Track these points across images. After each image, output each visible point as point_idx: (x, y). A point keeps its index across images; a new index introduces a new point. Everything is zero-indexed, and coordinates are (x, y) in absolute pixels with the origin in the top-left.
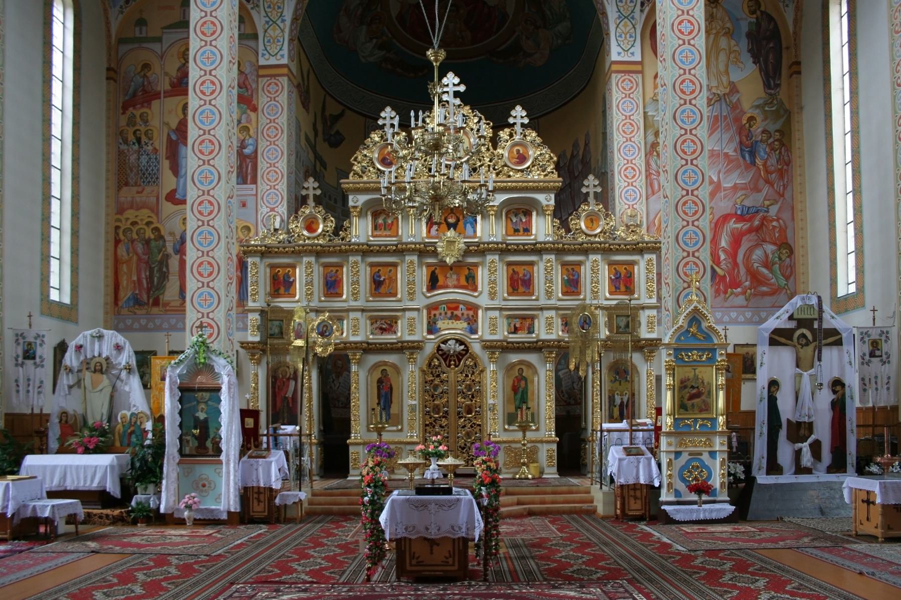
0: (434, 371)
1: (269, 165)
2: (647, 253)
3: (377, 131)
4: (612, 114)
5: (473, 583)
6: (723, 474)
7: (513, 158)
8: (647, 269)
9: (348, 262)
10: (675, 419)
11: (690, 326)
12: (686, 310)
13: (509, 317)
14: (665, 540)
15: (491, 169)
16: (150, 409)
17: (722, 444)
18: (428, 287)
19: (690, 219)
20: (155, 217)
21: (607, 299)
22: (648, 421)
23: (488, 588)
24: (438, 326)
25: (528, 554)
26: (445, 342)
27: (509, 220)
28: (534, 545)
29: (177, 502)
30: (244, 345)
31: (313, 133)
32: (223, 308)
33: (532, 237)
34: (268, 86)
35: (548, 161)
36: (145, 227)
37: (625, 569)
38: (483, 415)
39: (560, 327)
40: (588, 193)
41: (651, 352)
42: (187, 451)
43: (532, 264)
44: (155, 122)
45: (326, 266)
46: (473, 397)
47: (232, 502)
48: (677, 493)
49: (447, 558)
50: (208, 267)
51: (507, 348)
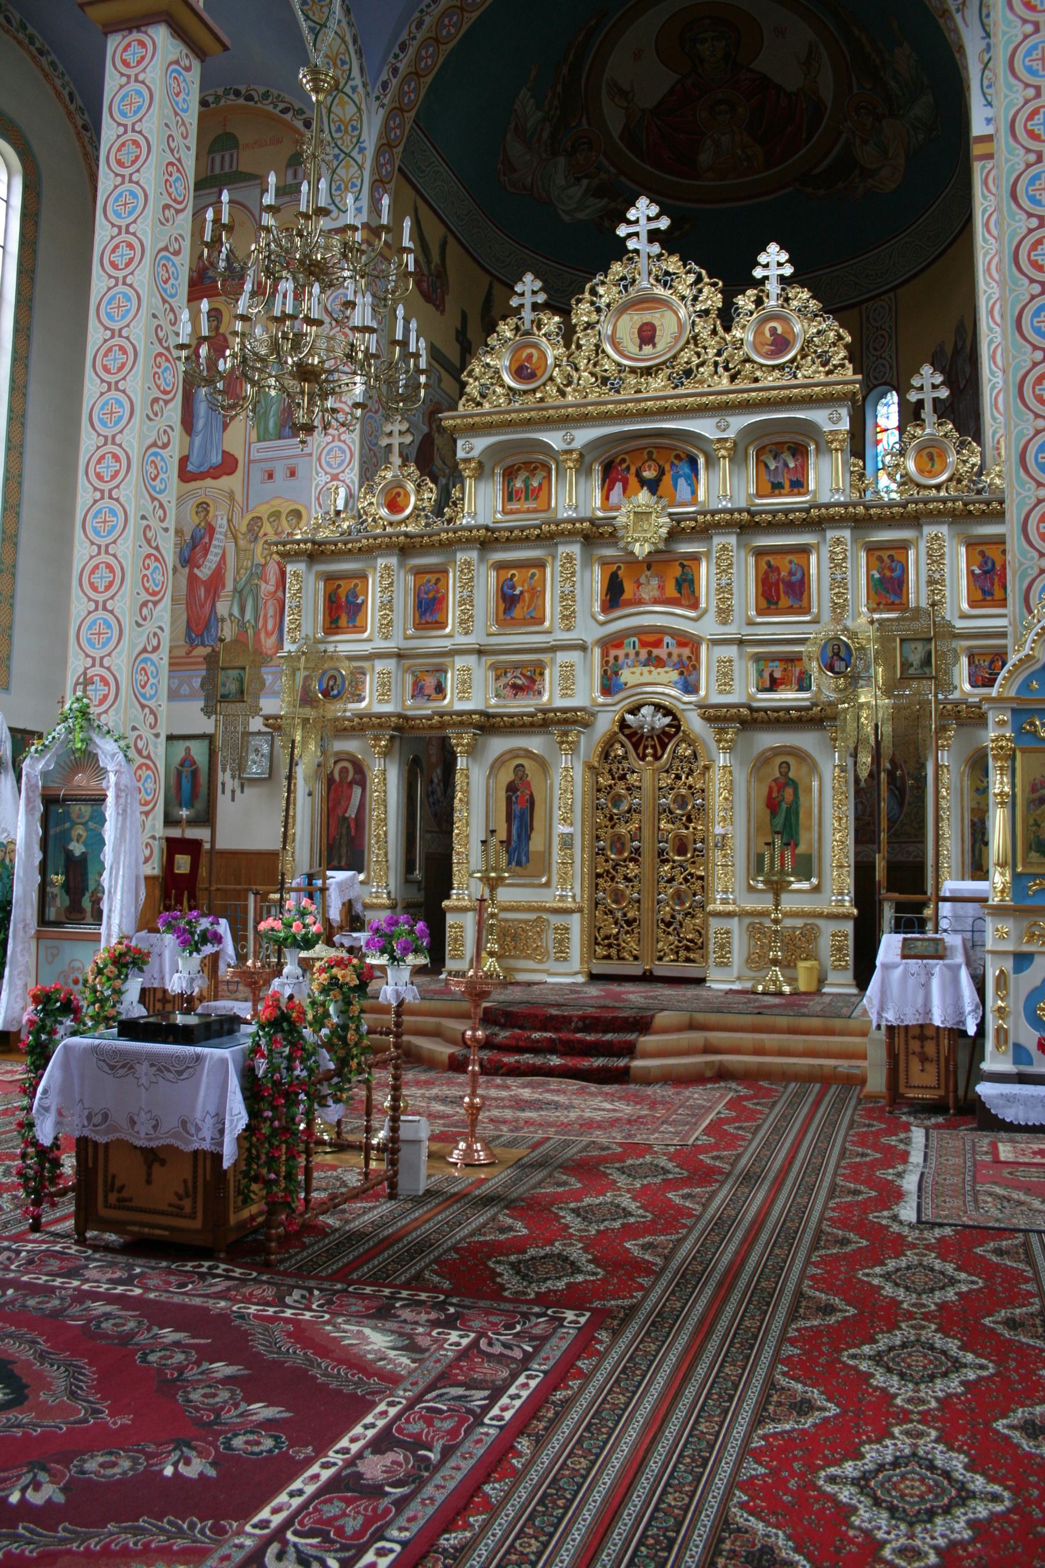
0: (614, 767)
3: (509, 320)
7: (763, 344)
10: (1016, 876)
13: (757, 658)
15: (720, 370)
18: (603, 602)
21: (964, 616)
27: (762, 467)
31: (458, 347)
35: (834, 344)
43: (804, 550)
45: (418, 572)
48: (1020, 1054)
49: (181, 1199)
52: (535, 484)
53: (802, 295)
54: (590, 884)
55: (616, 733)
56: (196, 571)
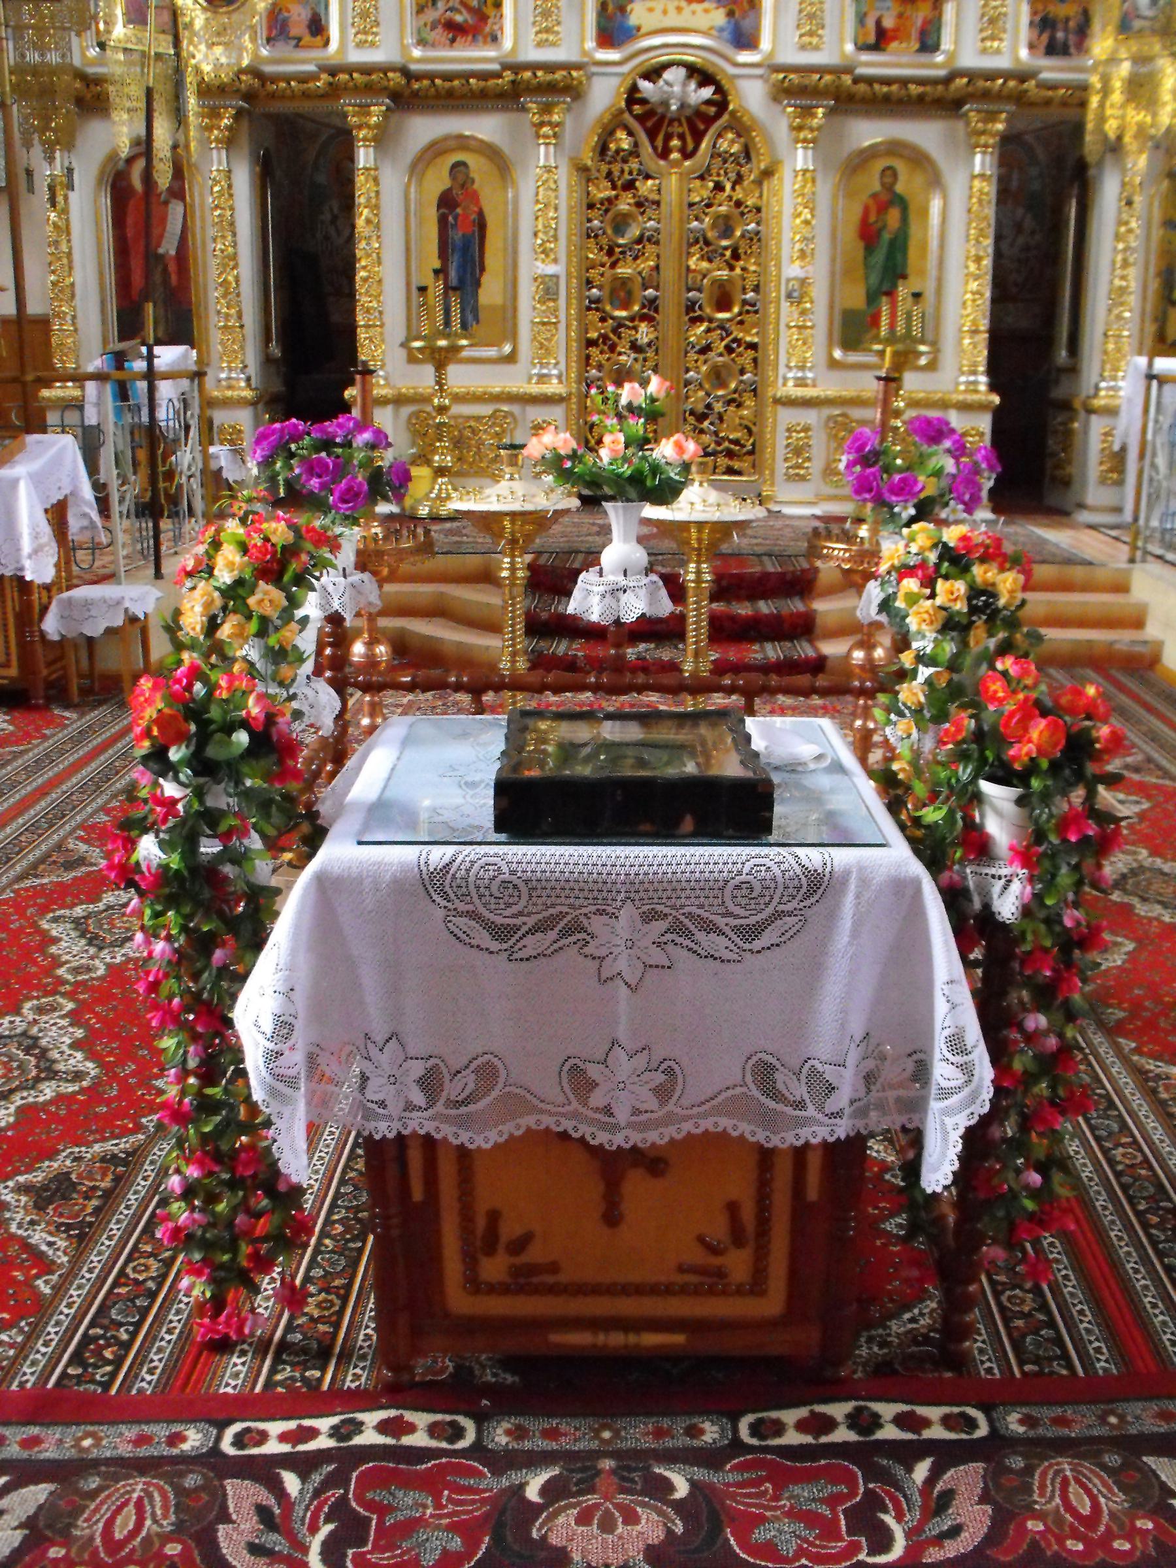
0: (616, 168)
26: (653, 73)
38: (766, 315)
46: (736, 256)
54: (579, 356)
55: (621, 112)
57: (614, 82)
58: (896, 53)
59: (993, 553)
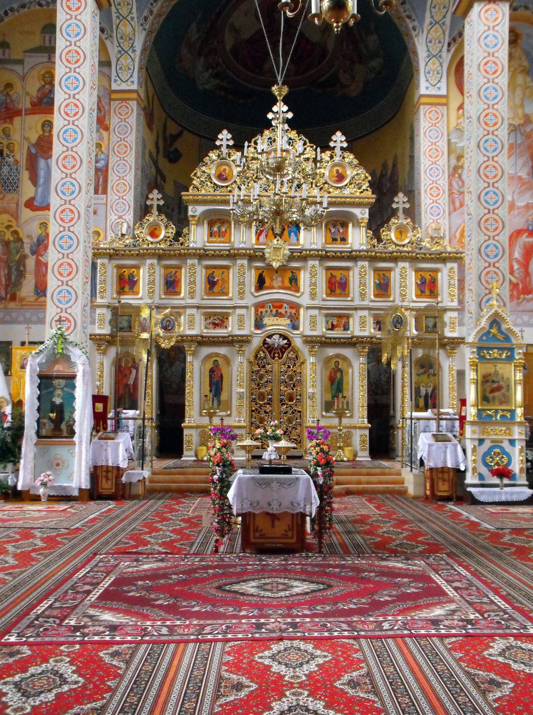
0: (260, 362)
1: (118, 178)
2: (449, 262)
4: (419, 140)
5: (310, 554)
6: (522, 461)
8: (450, 276)
9: (186, 264)
10: (478, 410)
11: (491, 327)
12: (487, 314)
13: (326, 316)
14: (473, 519)
16: (10, 394)
17: (520, 433)
19: (492, 234)
20: (14, 221)
22: (451, 411)
23: (324, 558)
24: (264, 322)
25: (353, 530)
26: (270, 337)
27: (328, 230)
28: (356, 521)
29: (33, 480)
30: (94, 338)
32: (80, 305)
33: (349, 246)
34: (119, 108)
35: (364, 180)
36: (5, 230)
37: (443, 544)
38: (303, 403)
39: (372, 325)
40: (397, 209)
41: (453, 349)
42: (44, 432)
43: (348, 269)
44: (16, 137)
45: (166, 267)
46: (294, 386)
47: (83, 480)
50: (67, 267)
51: (325, 343)
52: (224, 230)
53: (350, 157)
56: (40, 258)
57: (259, 338)
58: (337, 330)
59: (323, 444)
